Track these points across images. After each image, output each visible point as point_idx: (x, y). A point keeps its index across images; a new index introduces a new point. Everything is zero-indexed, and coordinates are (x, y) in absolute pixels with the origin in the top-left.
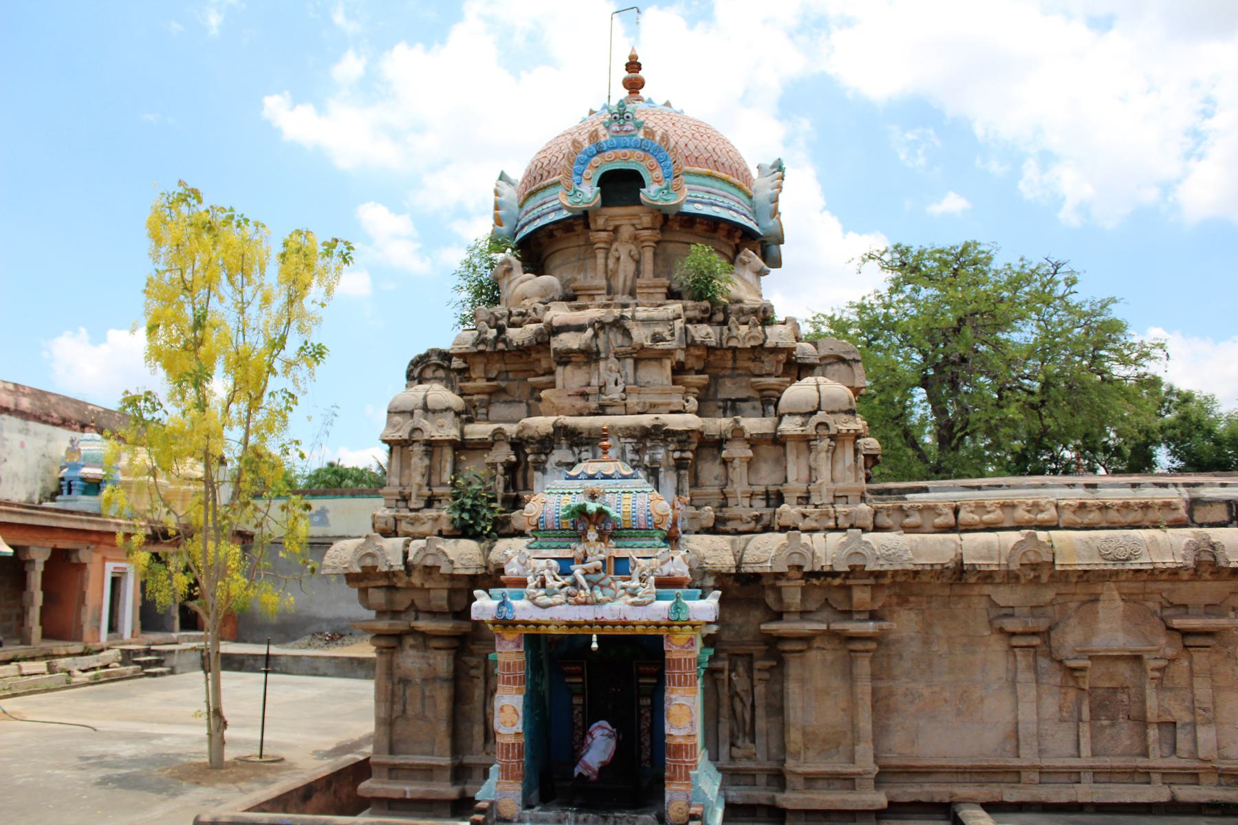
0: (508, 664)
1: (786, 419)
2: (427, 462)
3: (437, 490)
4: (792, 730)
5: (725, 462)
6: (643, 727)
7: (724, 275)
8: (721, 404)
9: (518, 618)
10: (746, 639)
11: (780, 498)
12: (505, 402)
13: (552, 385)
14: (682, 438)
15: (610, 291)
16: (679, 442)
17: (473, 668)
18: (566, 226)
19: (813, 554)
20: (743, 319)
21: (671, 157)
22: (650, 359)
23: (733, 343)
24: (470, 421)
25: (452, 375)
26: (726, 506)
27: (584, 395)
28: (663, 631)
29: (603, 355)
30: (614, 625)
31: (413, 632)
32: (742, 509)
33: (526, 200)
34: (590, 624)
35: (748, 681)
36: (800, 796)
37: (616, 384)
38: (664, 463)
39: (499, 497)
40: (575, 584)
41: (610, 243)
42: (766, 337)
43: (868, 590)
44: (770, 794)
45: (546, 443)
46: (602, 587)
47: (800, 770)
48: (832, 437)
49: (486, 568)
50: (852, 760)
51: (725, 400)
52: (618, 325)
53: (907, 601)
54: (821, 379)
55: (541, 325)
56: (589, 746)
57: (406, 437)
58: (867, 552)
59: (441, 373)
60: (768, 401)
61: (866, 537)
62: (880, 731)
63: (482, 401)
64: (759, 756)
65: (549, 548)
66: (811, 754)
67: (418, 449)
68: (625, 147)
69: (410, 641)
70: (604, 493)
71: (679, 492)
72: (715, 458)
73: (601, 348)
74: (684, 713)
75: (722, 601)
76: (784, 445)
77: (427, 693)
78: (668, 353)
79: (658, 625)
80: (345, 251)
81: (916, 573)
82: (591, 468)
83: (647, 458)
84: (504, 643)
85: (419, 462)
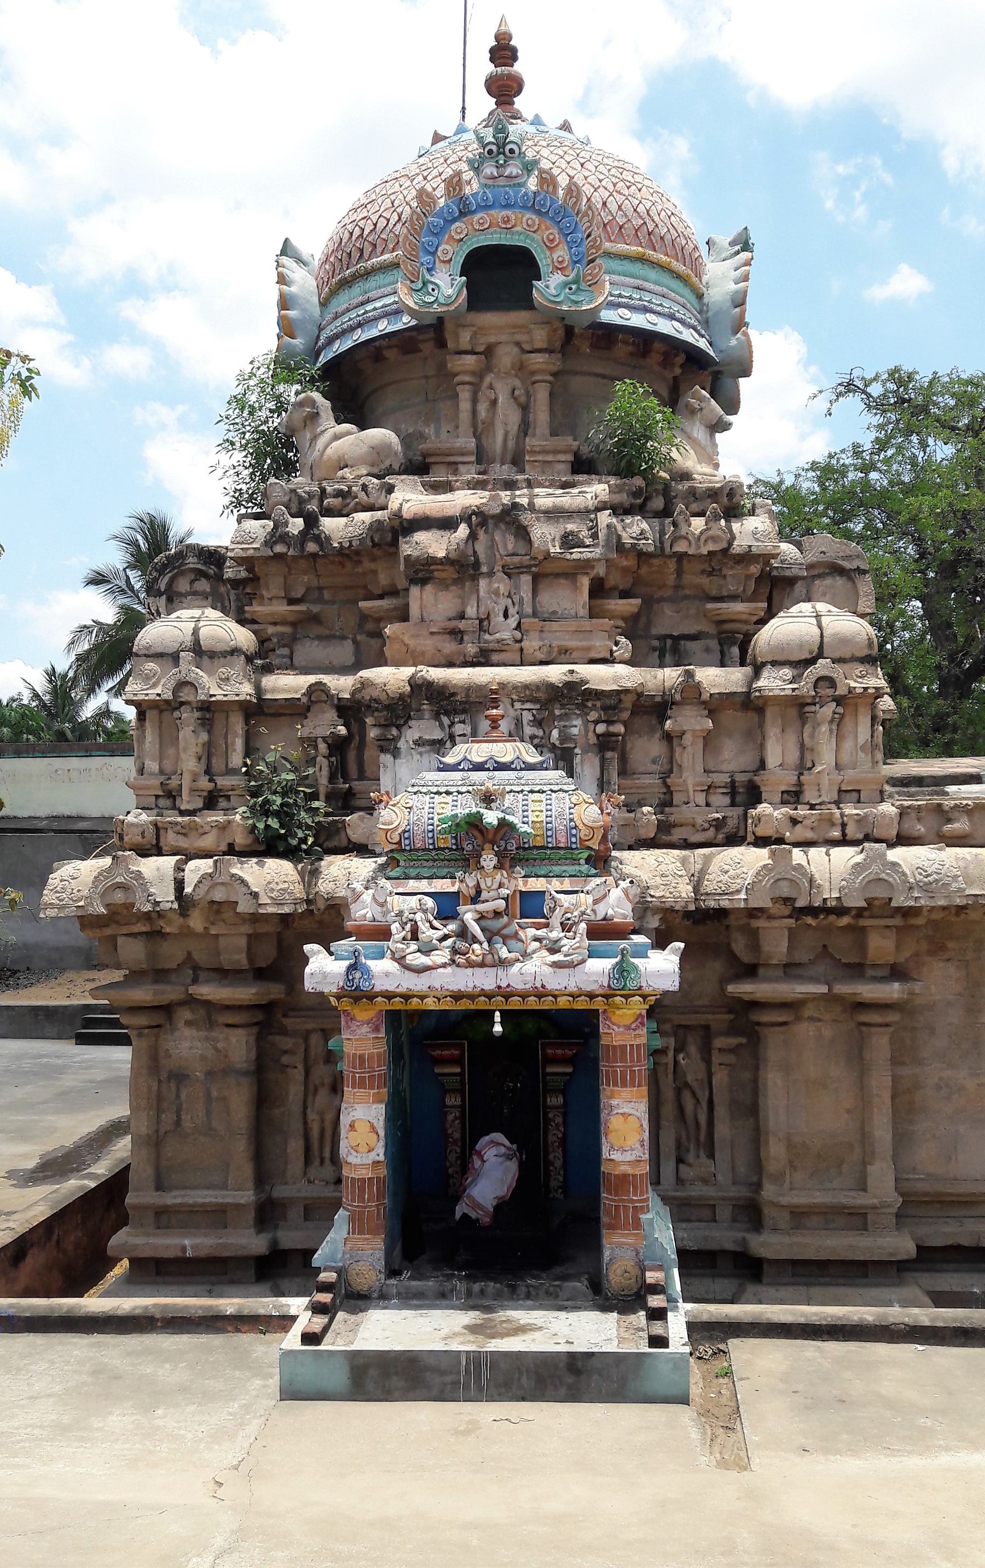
0: (362, 1057)
1: (765, 673)
2: (204, 736)
3: (224, 782)
4: (772, 1141)
5: (668, 737)
6: (551, 1138)
7: (667, 434)
8: (656, 643)
9: (377, 989)
10: (700, 1003)
11: (754, 796)
12: (319, 638)
13: (403, 616)
14: (610, 702)
15: (482, 457)
16: (605, 708)
17: (286, 1052)
18: (403, 342)
19: (811, 881)
20: (695, 507)
21: (584, 225)
22: (557, 575)
23: (680, 547)
24: (268, 669)
25: (222, 589)
26: (670, 804)
27: (457, 635)
28: (599, 1004)
29: (484, 569)
30: (524, 996)
31: (191, 1001)
32: (696, 810)
33: (334, 292)
34: (489, 996)
35: (703, 1066)
36: (786, 1240)
37: (506, 616)
38: (581, 741)
39: (322, 791)
40: (463, 933)
41: (480, 375)
42: (733, 538)
43: (892, 934)
44: (740, 1235)
45: (398, 710)
46: (505, 939)
47: (784, 1200)
48: (839, 700)
49: (308, 902)
50: (862, 1187)
51: (663, 638)
52: (510, 518)
53: (942, 948)
54: (822, 607)
55: (379, 515)
56: (478, 1174)
57: (168, 695)
58: (895, 879)
59: (203, 585)
60: (734, 644)
61: (897, 854)
62: (902, 1139)
63: (281, 636)
64: (719, 1178)
65: (418, 877)
66: (799, 1176)
67: (188, 716)
68: (507, 206)
69: (185, 1014)
70: (503, 794)
71: (602, 785)
72: (652, 731)
73: (482, 557)
74: (626, 1128)
75: (685, 958)
76: (760, 711)
77: (215, 1094)
78: (586, 565)
79: (592, 996)
80: (25, 374)
81: (961, 909)
82: (479, 751)
83: (555, 733)
84: (354, 1025)
85: (191, 740)
